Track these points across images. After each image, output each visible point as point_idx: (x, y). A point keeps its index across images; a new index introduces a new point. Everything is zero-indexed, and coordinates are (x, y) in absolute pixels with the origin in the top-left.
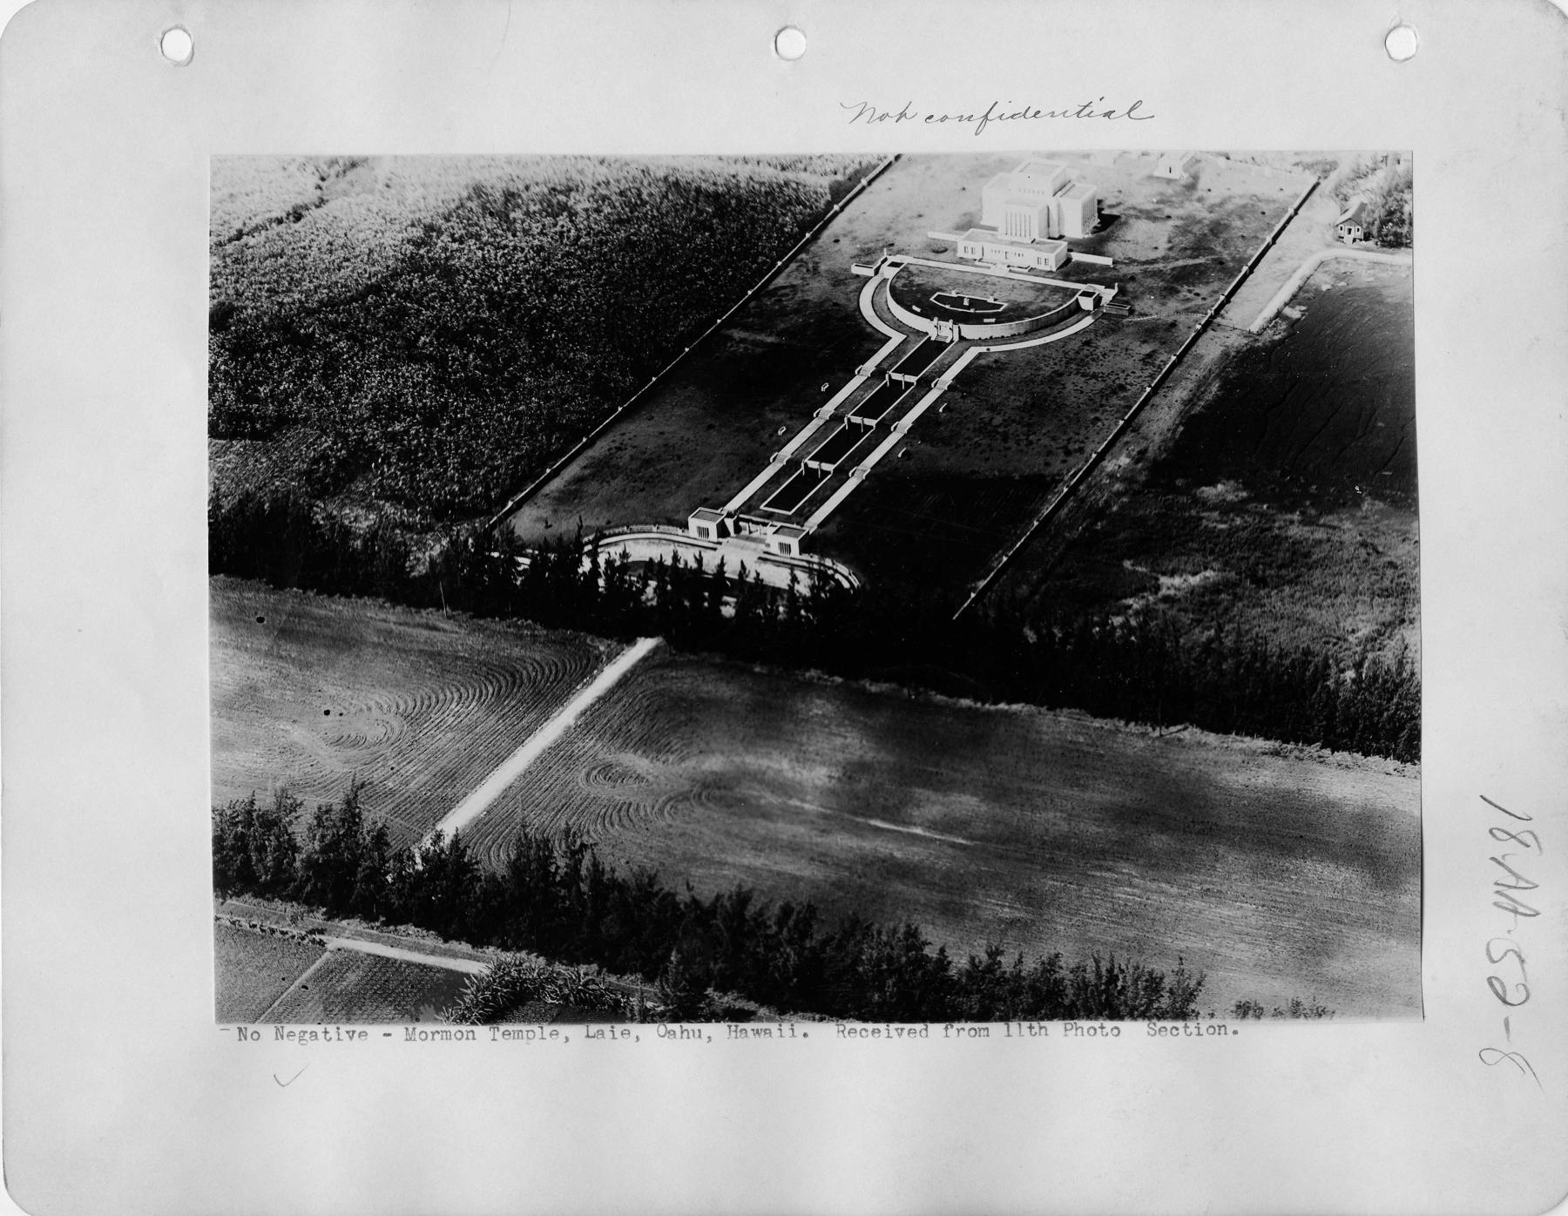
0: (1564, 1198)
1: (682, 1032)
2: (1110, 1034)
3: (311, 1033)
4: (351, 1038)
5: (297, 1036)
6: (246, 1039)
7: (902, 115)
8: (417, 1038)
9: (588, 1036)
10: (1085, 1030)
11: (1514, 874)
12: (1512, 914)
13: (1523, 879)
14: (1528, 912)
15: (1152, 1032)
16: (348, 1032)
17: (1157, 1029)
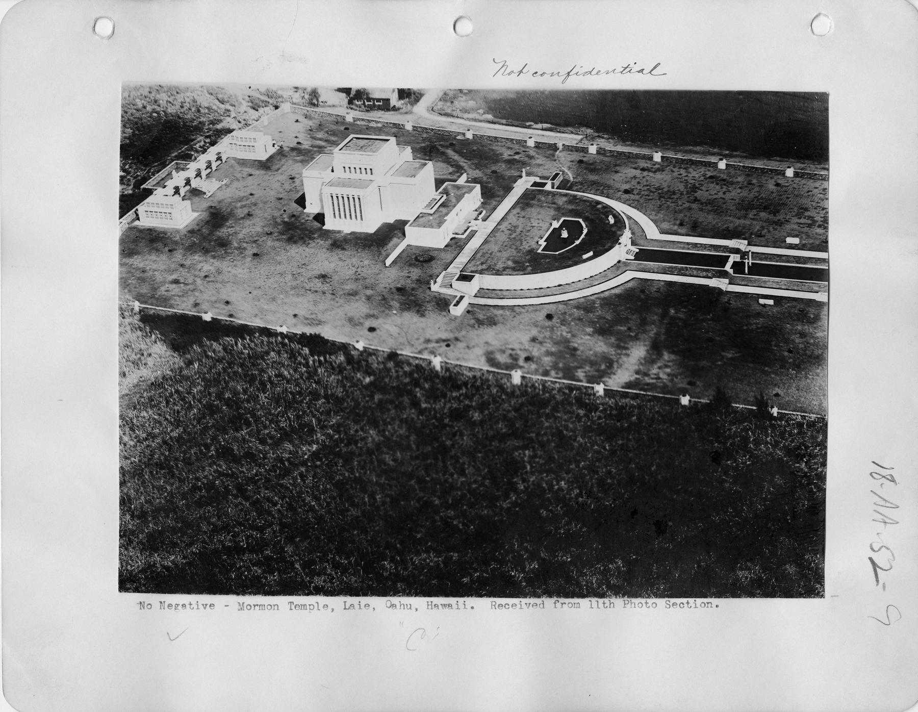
0: (916, 703)
1: (610, 604)
2: (651, 607)
3: (182, 605)
4: (205, 608)
5: (174, 607)
6: (144, 608)
7: (521, 72)
8: (245, 608)
9: (345, 609)
10: (636, 604)
11: (884, 500)
12: (883, 524)
13: (889, 502)
14: (892, 522)
15: (668, 606)
16: (203, 605)
17: (671, 604)
